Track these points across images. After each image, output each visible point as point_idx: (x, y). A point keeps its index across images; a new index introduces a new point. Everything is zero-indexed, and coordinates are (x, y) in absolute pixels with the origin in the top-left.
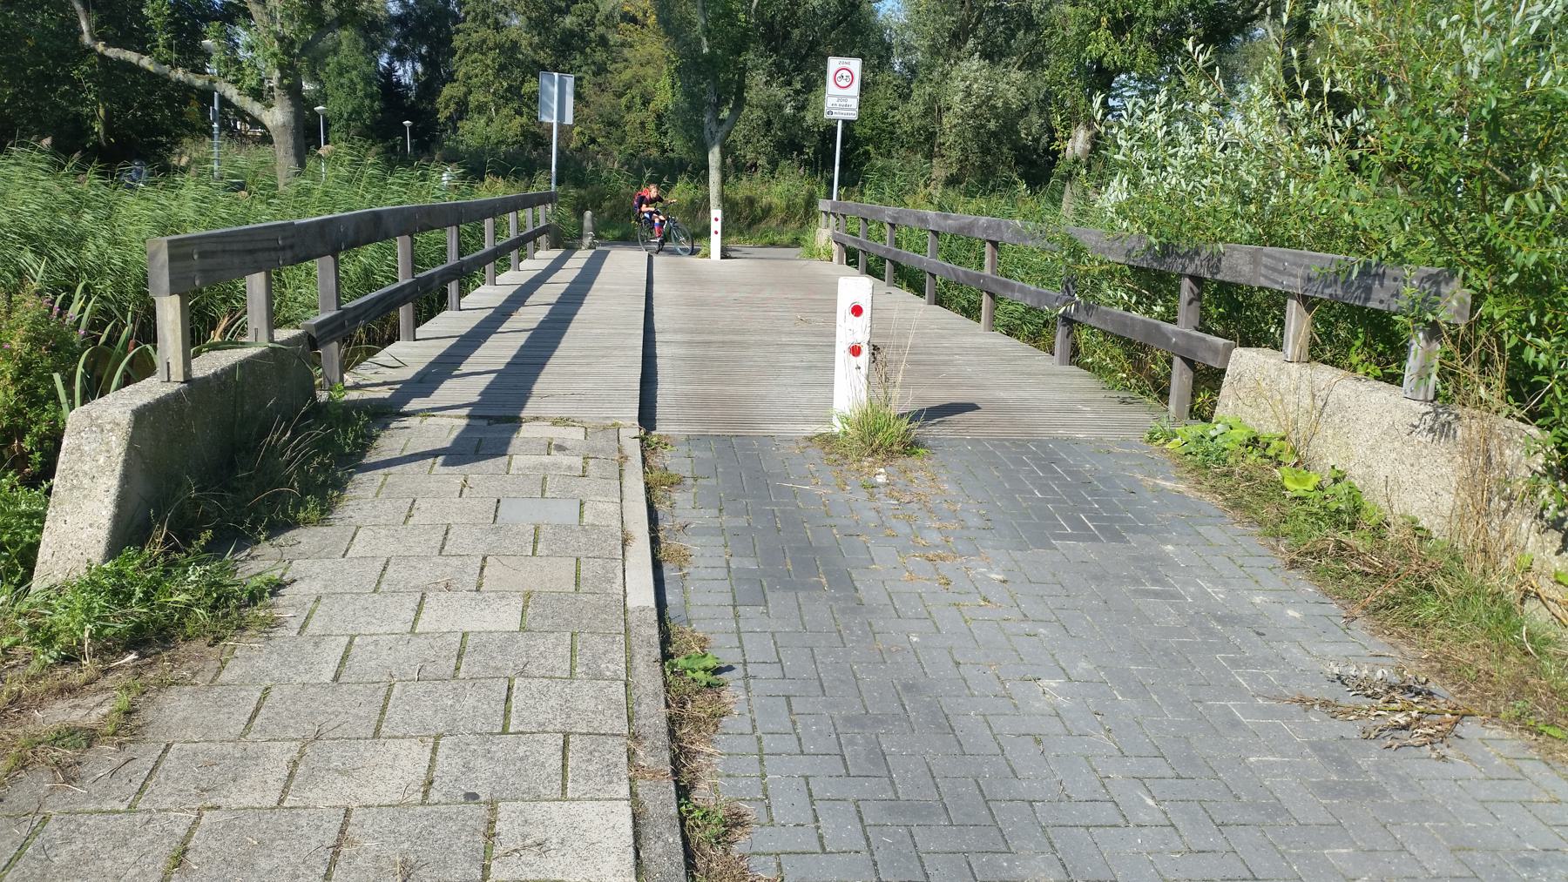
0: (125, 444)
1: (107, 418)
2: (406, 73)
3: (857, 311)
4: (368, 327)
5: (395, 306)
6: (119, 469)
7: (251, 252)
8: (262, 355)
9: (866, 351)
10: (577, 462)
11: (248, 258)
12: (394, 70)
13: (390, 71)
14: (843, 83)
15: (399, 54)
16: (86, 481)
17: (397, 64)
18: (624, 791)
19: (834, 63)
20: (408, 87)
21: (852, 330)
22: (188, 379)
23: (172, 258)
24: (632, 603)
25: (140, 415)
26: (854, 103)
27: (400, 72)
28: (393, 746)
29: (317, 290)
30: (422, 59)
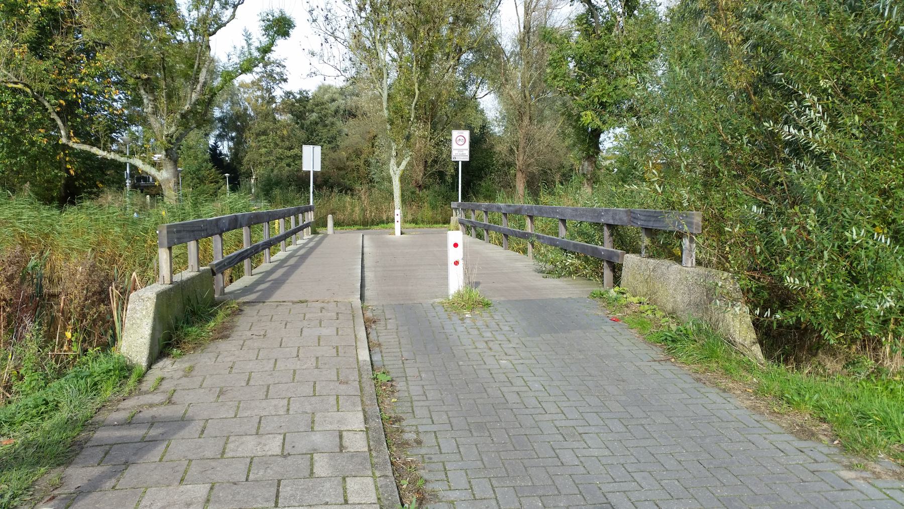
0: (153, 306)
1: (145, 296)
2: (225, 148)
3: (456, 245)
4: (234, 264)
5: (242, 259)
6: (152, 315)
7: (193, 231)
8: (192, 279)
9: (461, 262)
10: (334, 314)
11: (192, 234)
12: (217, 147)
13: (215, 147)
14: (461, 143)
15: (220, 137)
16: (138, 321)
17: (219, 143)
18: (360, 408)
19: (455, 133)
20: (226, 155)
21: (455, 254)
22: (172, 283)
23: (168, 232)
24: (360, 358)
25: (160, 296)
26: (467, 153)
27: (221, 148)
28: (274, 402)
29: (219, 249)
30: (232, 139)
